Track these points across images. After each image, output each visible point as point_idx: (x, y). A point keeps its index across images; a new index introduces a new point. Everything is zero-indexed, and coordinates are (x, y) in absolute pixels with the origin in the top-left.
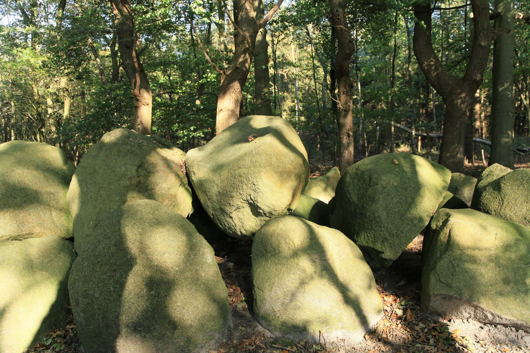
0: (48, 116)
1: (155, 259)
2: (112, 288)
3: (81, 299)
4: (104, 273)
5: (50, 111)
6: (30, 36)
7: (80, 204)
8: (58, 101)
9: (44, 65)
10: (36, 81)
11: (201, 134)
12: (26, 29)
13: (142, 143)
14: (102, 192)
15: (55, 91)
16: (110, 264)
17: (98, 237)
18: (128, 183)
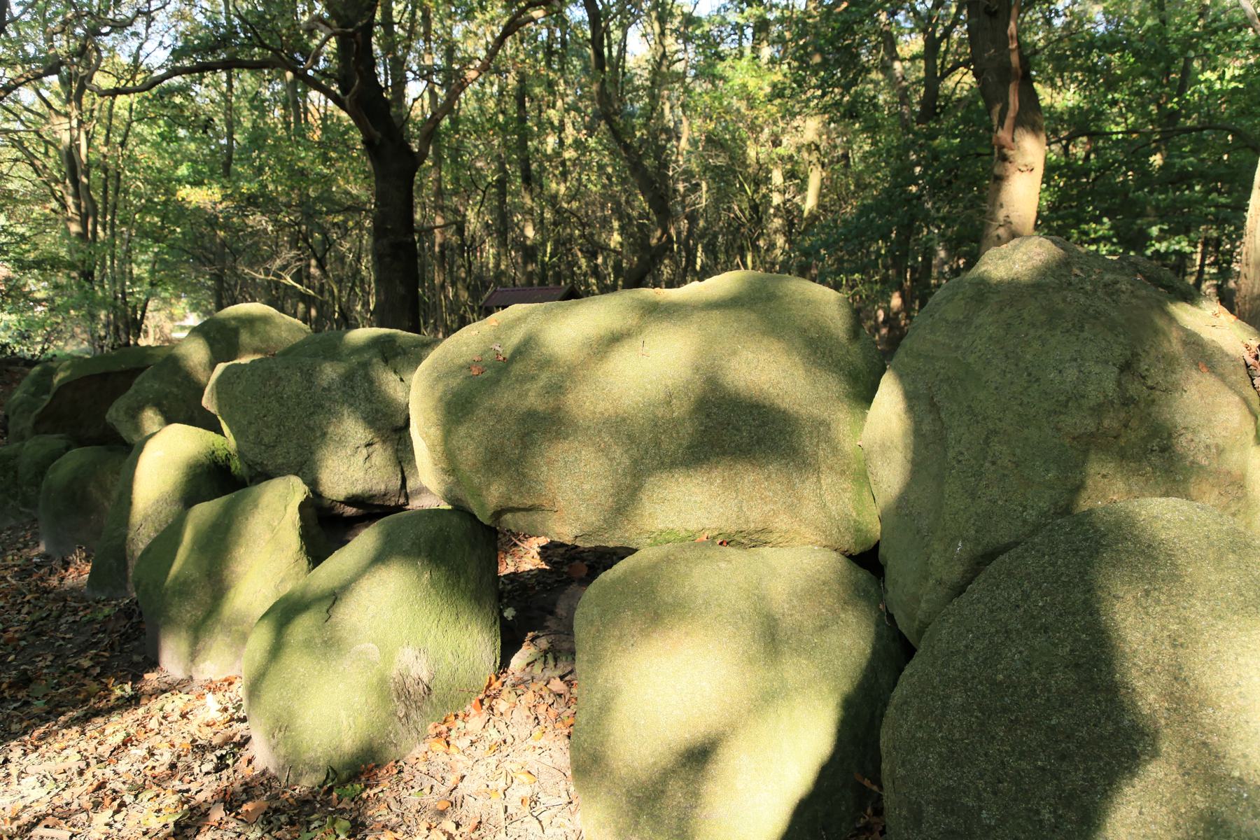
0: (772, 211)
1: (1233, 754)
2: (1046, 815)
3: (931, 809)
4: (1022, 753)
5: (777, 199)
6: (749, 32)
7: (909, 466)
8: (795, 175)
9: (778, 92)
10: (754, 128)
11: (1184, 244)
12: (746, 14)
13: (1116, 282)
14: (998, 447)
15: (792, 151)
16: (1052, 728)
17: (1003, 616)
18: (1090, 424)
